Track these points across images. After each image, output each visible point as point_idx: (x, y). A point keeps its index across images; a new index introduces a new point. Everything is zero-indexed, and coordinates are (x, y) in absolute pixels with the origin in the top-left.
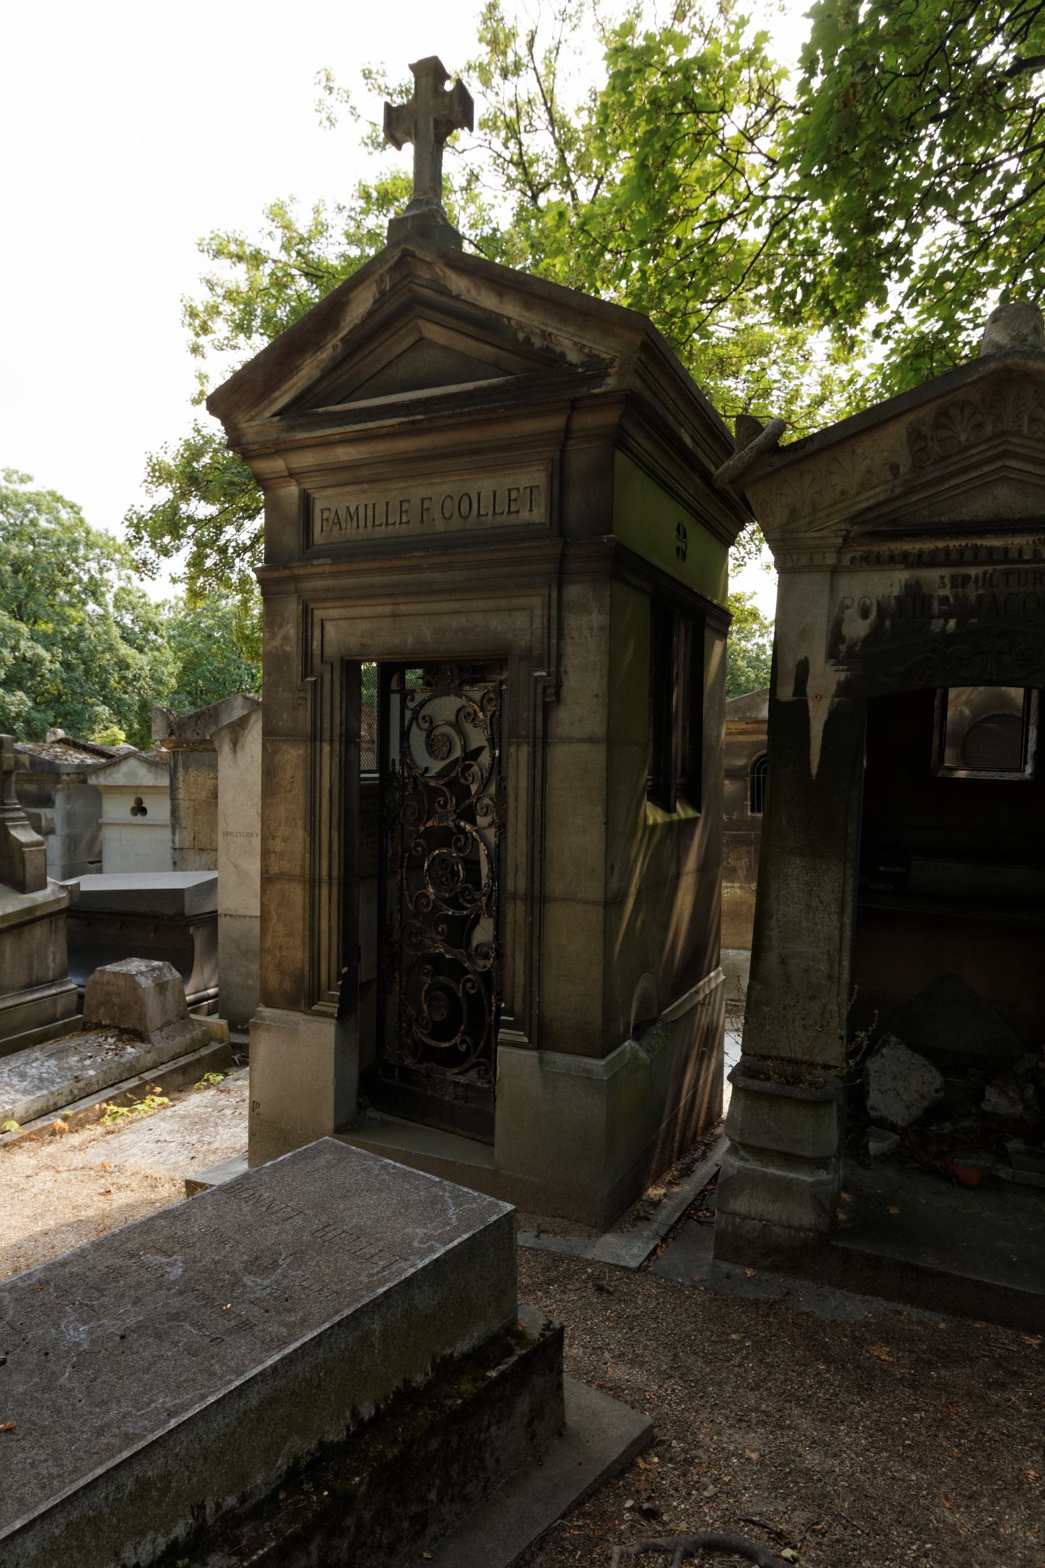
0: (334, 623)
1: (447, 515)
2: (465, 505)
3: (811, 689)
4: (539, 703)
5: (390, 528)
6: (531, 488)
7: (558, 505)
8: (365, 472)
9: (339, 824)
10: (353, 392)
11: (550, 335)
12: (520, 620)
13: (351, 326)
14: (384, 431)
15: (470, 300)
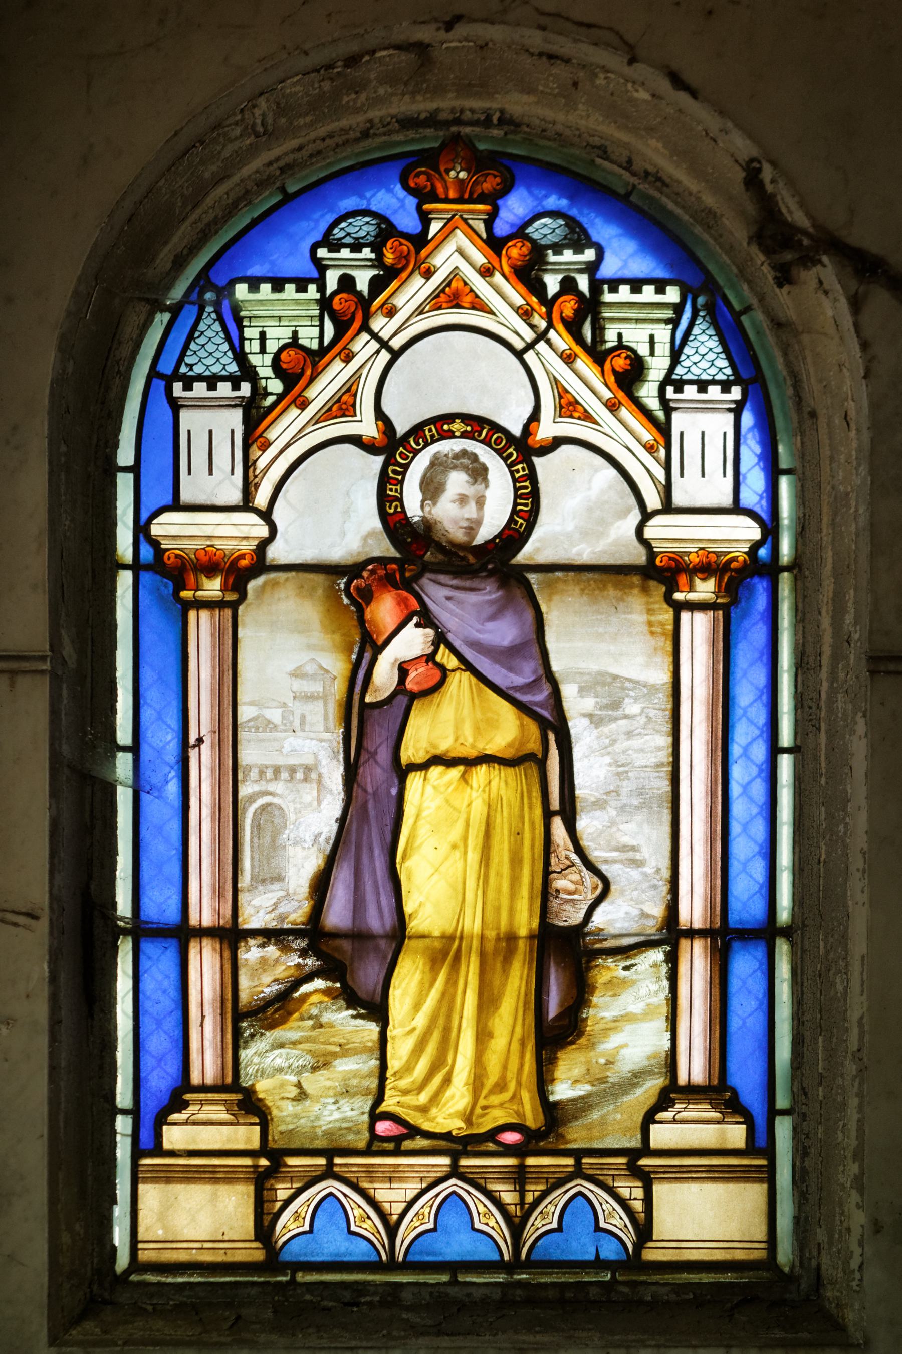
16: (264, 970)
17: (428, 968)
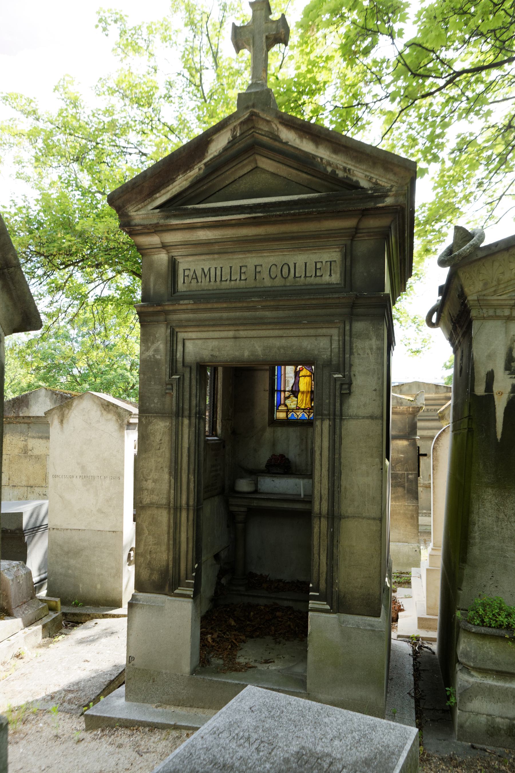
0: (192, 341)
1: (273, 276)
2: (285, 270)
3: (496, 388)
4: (338, 394)
5: (233, 283)
6: (331, 262)
7: (348, 273)
8: (216, 247)
9: (194, 471)
10: (209, 197)
11: (349, 170)
12: (323, 343)
13: (212, 156)
14: (233, 222)
15: (294, 145)
16: (287, 394)
17: (82, 626)
